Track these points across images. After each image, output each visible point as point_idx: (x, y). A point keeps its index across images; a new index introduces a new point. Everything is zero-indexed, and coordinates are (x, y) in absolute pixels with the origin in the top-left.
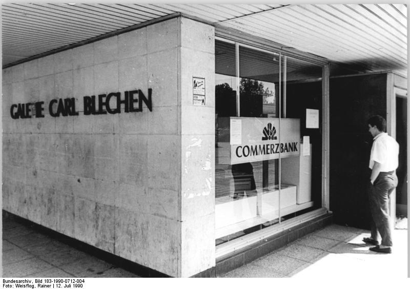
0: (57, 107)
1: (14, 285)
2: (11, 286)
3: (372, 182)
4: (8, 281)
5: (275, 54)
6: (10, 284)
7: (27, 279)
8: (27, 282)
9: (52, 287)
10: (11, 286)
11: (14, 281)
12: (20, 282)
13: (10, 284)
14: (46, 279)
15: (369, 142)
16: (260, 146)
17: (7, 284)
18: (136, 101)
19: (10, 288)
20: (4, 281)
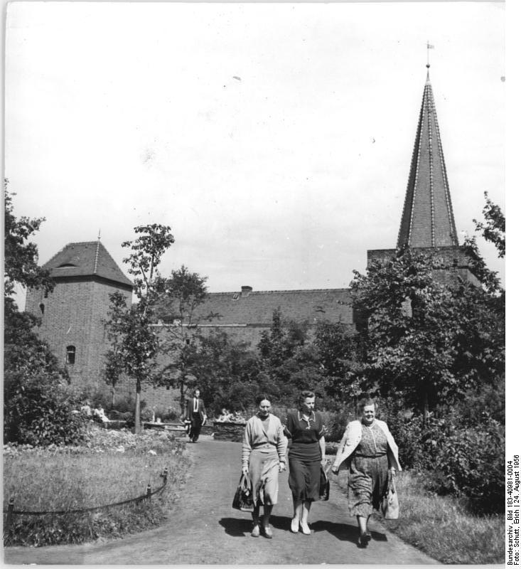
11: (510, 549)
12: (511, 541)
13: (514, 555)
17: (514, 559)
20: (510, 563)
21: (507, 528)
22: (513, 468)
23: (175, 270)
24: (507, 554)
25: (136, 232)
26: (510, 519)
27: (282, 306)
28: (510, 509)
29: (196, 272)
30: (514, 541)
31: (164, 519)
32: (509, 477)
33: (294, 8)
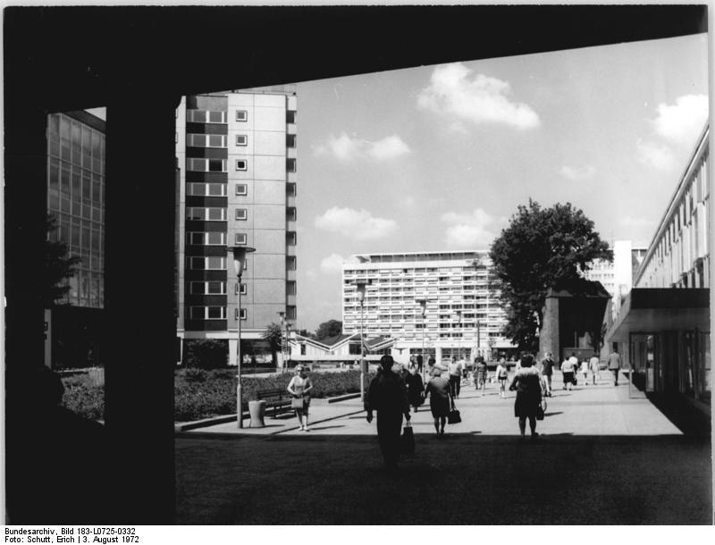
0: (564, 295)
1: (24, 537)
2: (19, 540)
3: (571, 296)
4: (14, 532)
5: (661, 356)
6: (17, 536)
7: (46, 527)
8: (48, 533)
9: (76, 542)
10: (19, 540)
11: (25, 532)
12: (35, 532)
13: (17, 536)
14: (81, 527)
15: (566, 289)
16: (346, 291)
17: (12, 536)
18: (254, 360)
19: (17, 543)
20: (7, 531)
21: (52, 527)
22: (122, 535)
23: (584, 213)
24: (18, 528)
25: (613, 275)
26: (63, 531)
27: (426, 330)
28: (76, 531)
29: (556, 203)
30: (35, 536)
31: (568, 203)
32: (116, 530)
33: (241, 165)
